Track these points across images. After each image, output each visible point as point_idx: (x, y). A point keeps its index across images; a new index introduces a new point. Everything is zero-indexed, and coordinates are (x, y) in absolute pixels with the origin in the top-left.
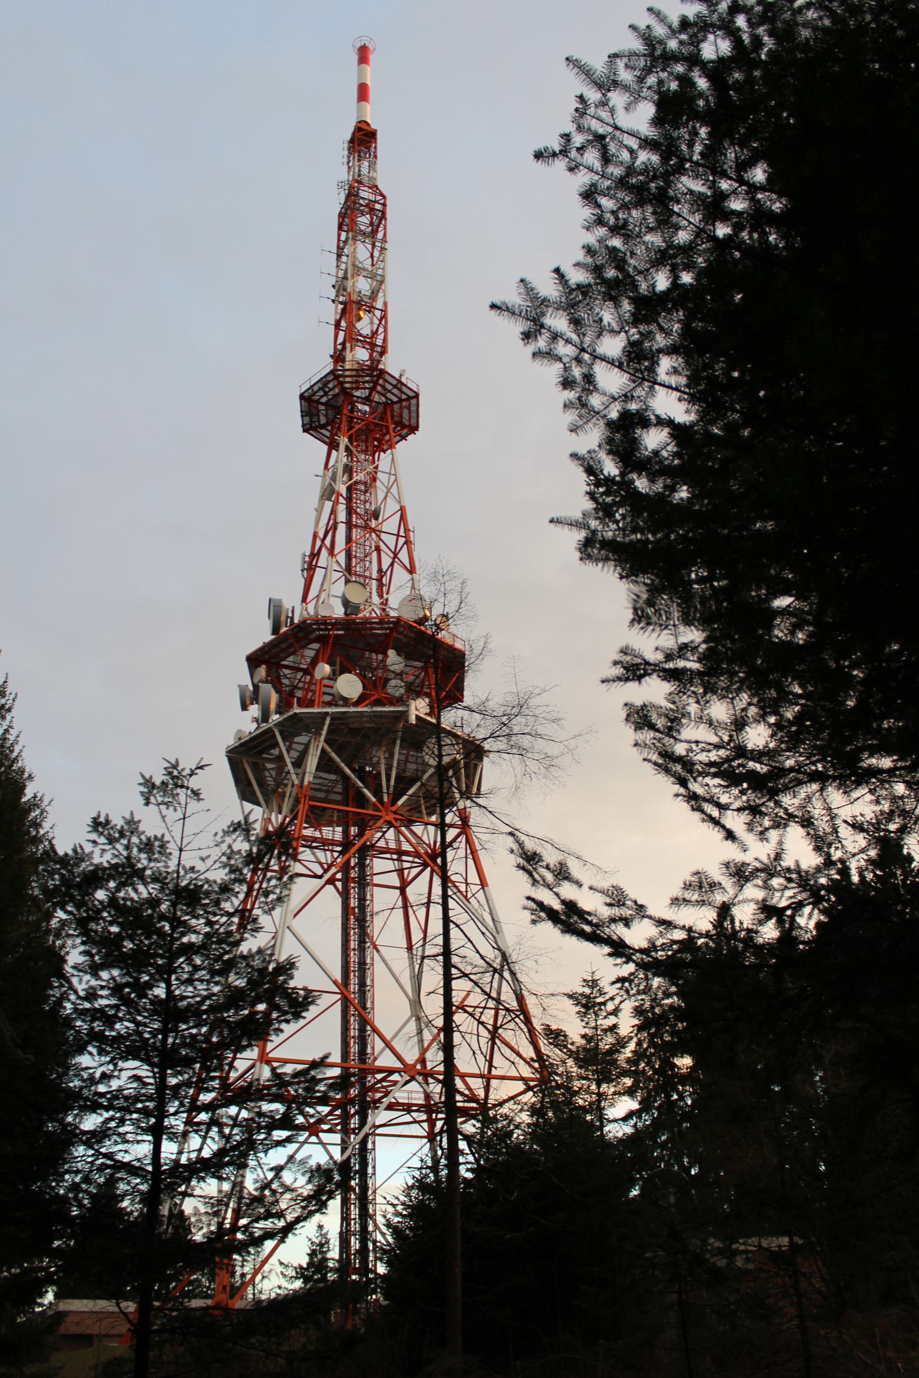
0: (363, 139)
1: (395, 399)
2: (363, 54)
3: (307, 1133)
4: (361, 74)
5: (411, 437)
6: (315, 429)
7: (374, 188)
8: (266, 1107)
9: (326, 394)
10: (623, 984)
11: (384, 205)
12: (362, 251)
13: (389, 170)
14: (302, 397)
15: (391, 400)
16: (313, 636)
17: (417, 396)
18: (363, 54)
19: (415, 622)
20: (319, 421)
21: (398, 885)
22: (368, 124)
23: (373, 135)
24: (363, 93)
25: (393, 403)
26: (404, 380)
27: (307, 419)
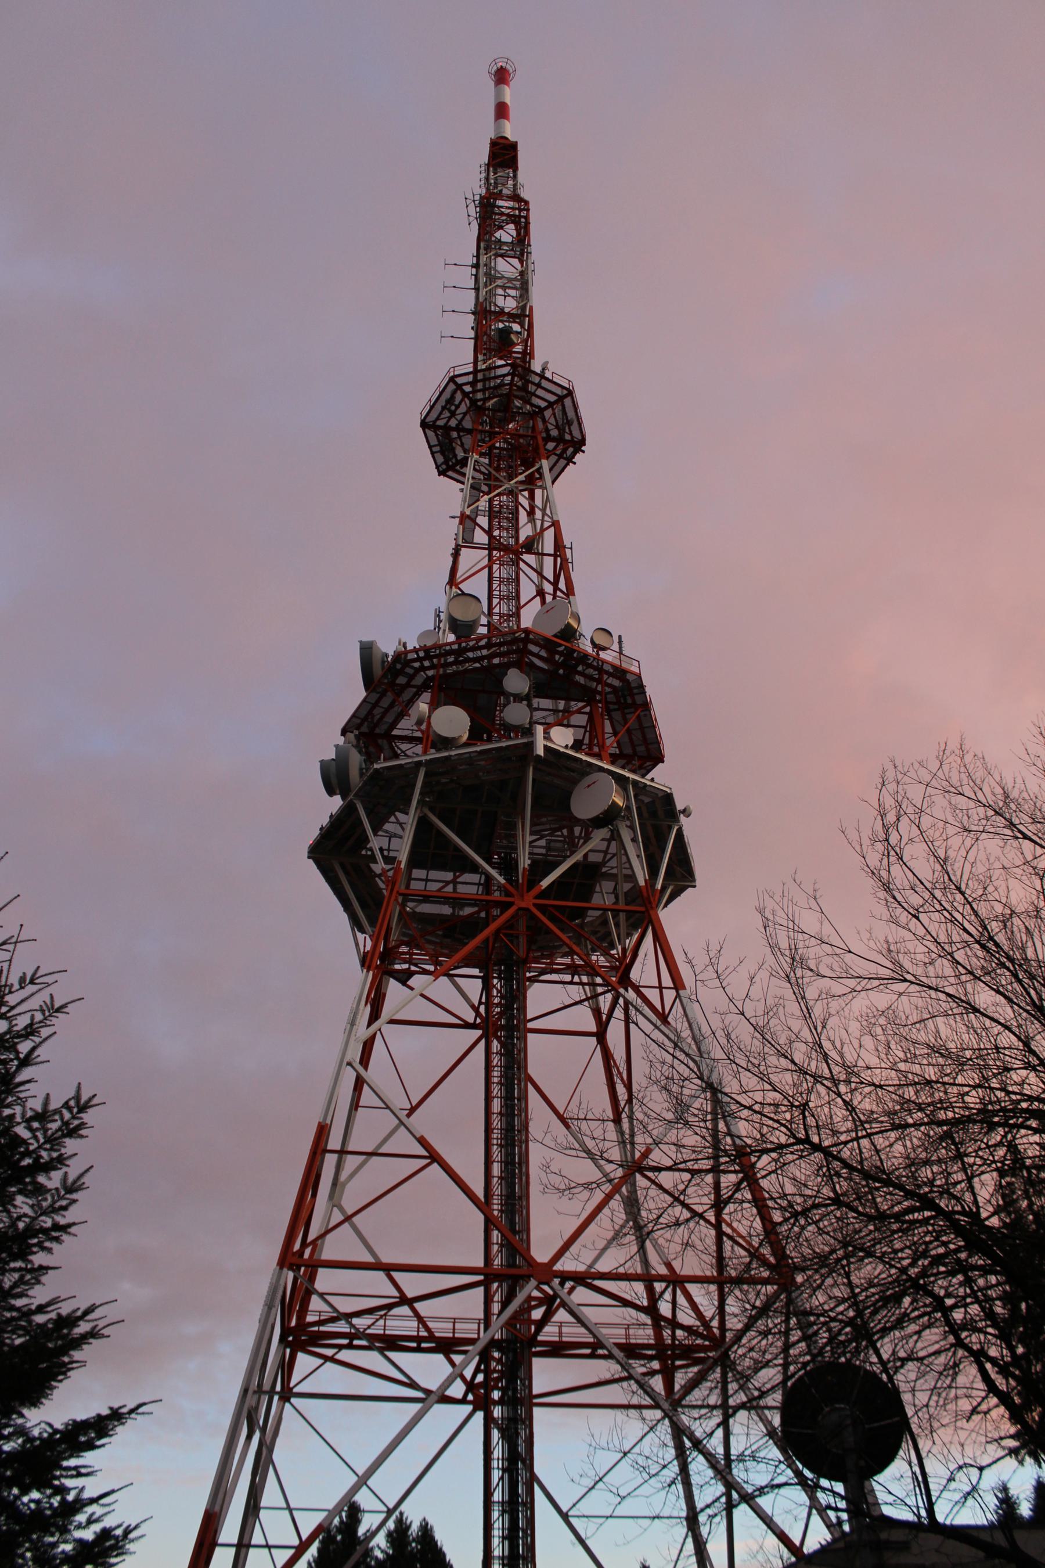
0: (503, 155)
1: (543, 404)
2: (502, 76)
3: (987, 1223)
4: (498, 94)
5: (578, 458)
6: (452, 468)
7: (516, 197)
8: (11, 1430)
9: (453, 414)
10: (711, 1113)
11: (528, 210)
12: (507, 267)
13: (531, 177)
14: (424, 425)
15: (538, 407)
16: (419, 680)
17: (570, 393)
18: (502, 76)
19: (555, 636)
20: (455, 456)
21: (594, 1029)
22: (506, 138)
23: (513, 147)
24: (502, 111)
25: (542, 410)
26: (548, 375)
27: (440, 459)
